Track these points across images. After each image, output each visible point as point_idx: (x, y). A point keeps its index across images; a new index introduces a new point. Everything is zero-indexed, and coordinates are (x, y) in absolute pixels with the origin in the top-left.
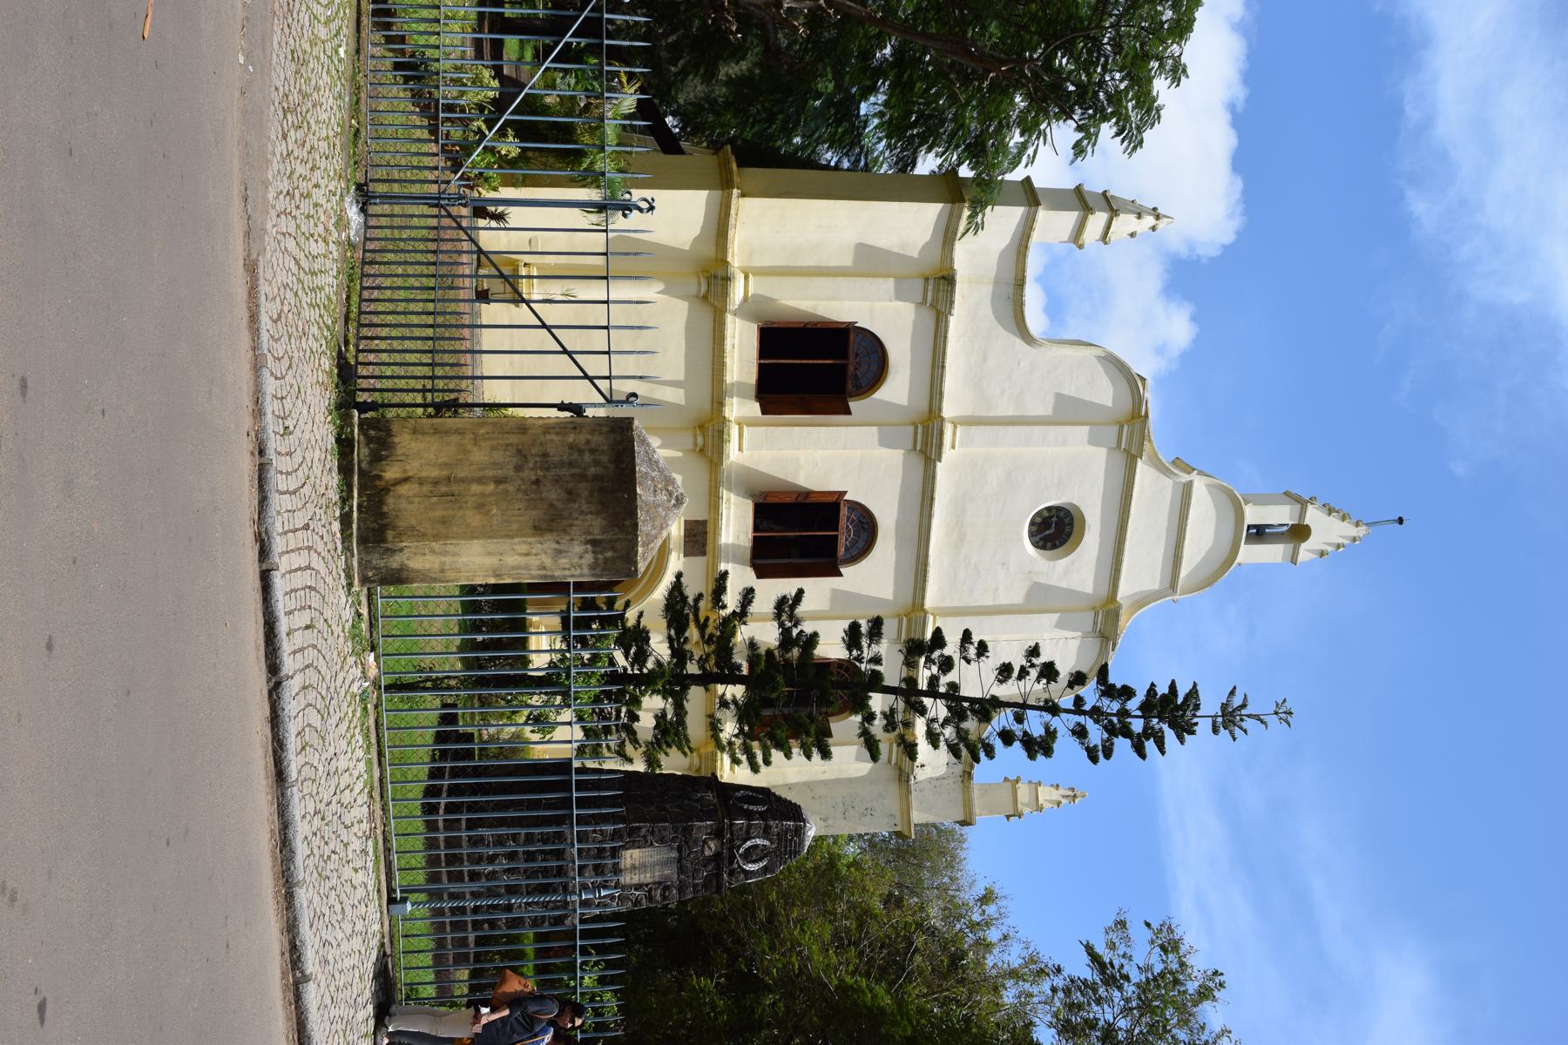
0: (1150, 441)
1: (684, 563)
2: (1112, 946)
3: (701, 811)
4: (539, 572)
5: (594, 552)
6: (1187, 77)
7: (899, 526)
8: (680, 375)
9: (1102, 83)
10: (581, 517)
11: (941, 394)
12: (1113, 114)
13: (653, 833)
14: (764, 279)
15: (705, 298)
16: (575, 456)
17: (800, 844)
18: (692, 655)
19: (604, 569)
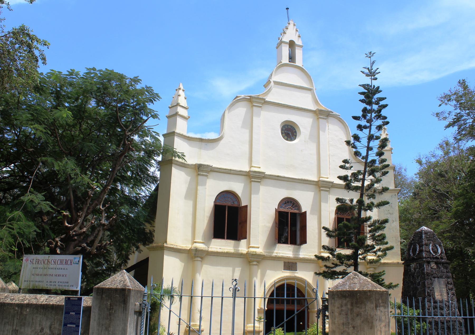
0: (259, 96)
1: (299, 271)
2: (445, 118)
3: (420, 269)
4: (387, 328)
5: (380, 307)
6: (138, 76)
7: (287, 189)
8: (231, 269)
9: (134, 107)
10: (367, 311)
11: (240, 171)
12: (144, 104)
13: (429, 287)
14: (196, 236)
15: (202, 258)
16: (343, 313)
17: (430, 233)
18: (344, 270)
19: (385, 303)
